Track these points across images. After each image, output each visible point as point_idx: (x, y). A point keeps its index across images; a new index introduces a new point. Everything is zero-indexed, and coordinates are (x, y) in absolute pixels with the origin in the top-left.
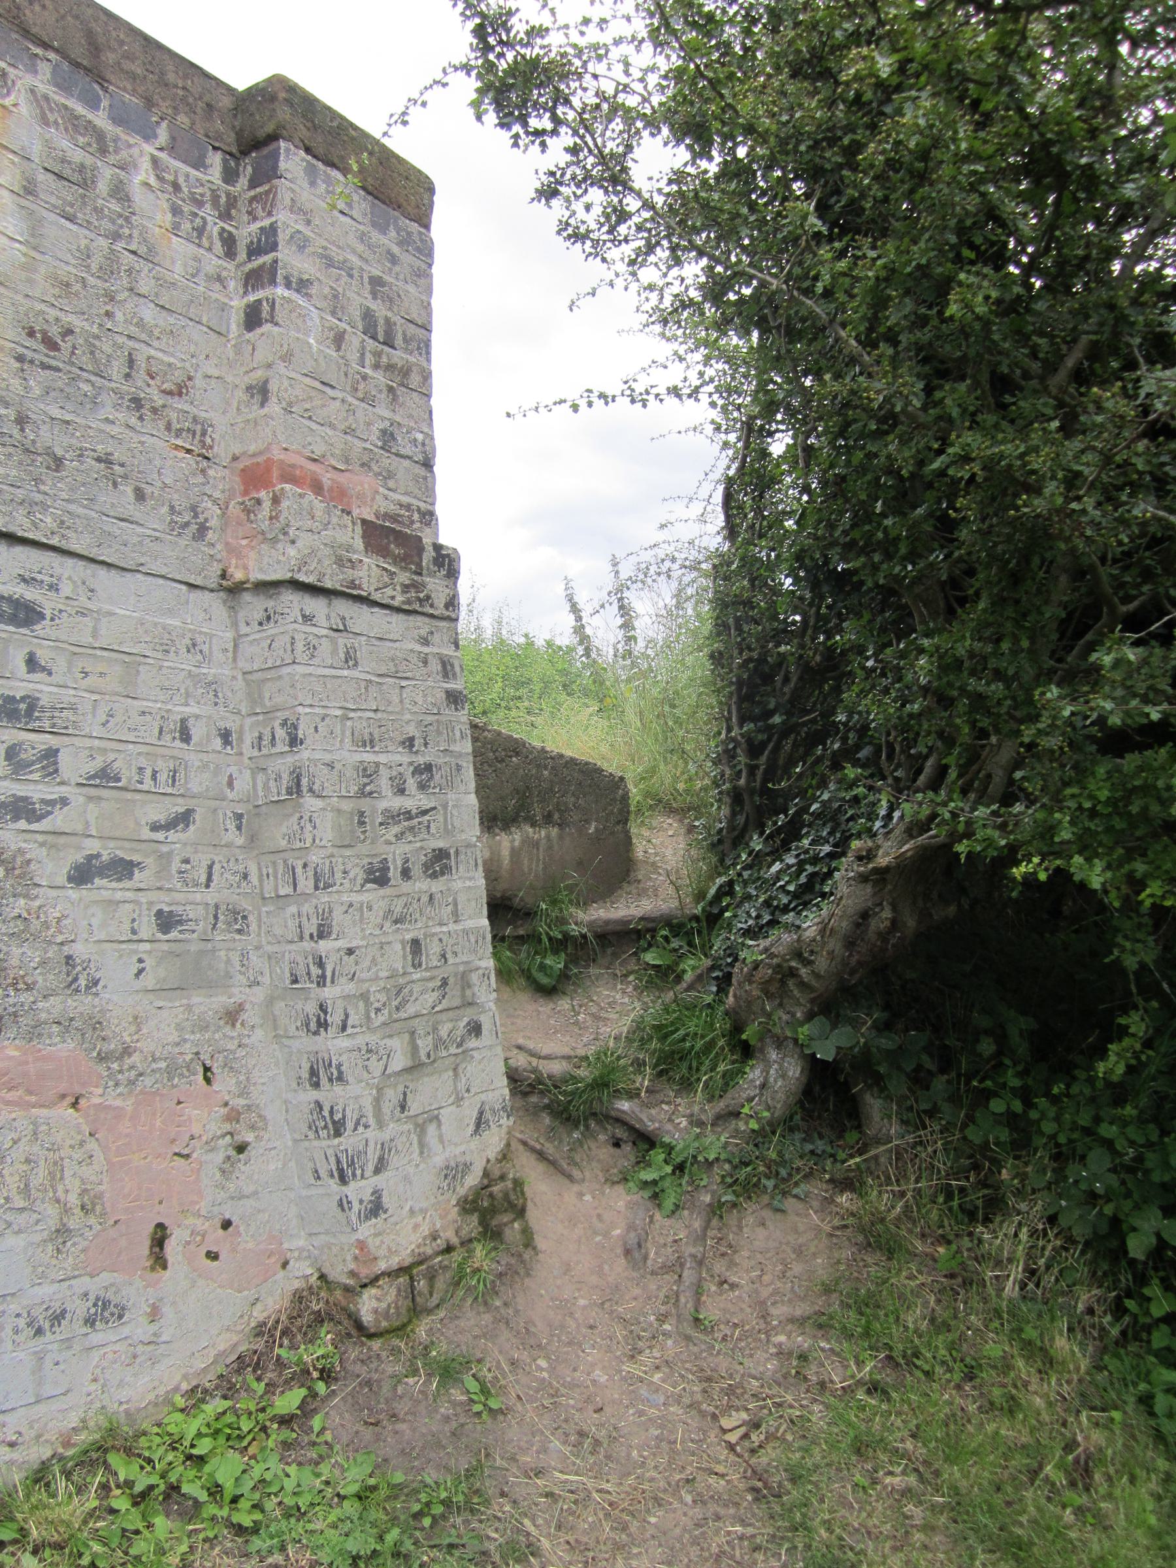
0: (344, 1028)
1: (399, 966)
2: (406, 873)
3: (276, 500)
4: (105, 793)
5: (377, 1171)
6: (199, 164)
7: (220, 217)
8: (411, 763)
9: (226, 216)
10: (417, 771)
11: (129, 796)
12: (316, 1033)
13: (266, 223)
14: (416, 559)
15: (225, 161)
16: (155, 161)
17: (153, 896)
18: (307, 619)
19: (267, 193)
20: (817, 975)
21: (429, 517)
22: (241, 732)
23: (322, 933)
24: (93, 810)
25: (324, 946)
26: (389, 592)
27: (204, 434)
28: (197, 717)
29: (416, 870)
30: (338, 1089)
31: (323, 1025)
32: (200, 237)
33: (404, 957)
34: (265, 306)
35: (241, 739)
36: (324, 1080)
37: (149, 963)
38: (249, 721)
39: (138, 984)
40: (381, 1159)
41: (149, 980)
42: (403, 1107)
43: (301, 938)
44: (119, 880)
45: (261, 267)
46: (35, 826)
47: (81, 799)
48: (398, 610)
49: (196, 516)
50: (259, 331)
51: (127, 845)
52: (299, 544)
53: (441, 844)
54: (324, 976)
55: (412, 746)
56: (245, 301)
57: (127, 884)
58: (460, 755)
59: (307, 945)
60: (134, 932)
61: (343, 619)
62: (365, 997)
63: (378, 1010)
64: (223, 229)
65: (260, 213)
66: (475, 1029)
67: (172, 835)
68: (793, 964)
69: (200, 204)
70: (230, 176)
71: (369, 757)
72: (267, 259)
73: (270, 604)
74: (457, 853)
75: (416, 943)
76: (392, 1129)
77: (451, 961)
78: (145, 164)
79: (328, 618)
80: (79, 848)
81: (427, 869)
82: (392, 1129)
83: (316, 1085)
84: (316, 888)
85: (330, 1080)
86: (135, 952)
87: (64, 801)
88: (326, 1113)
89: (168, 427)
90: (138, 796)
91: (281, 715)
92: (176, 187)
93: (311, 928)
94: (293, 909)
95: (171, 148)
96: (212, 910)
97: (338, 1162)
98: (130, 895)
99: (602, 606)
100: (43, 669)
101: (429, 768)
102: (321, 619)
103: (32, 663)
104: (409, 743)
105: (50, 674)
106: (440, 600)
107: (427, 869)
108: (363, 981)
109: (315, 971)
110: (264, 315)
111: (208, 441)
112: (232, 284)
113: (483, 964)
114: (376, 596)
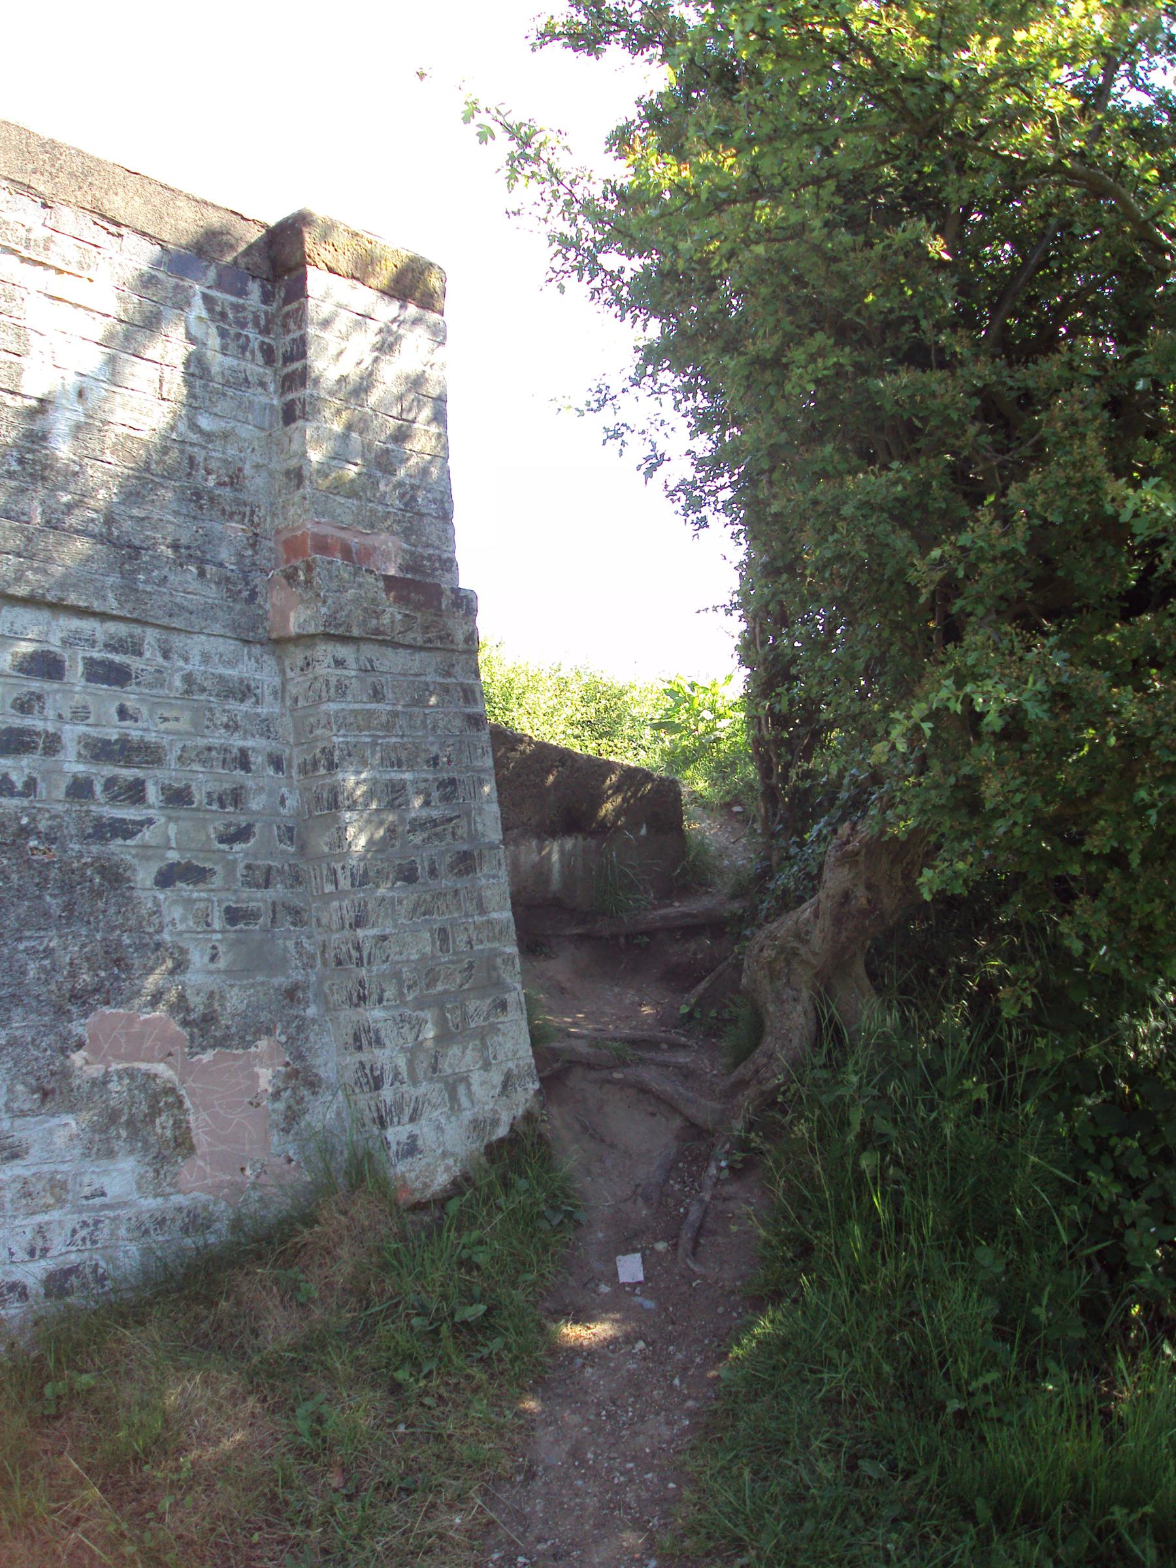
0: (380, 1001)
1: (428, 949)
2: (433, 872)
3: (309, 568)
4: (182, 813)
5: (412, 1120)
6: (242, 292)
7: (260, 333)
8: (435, 780)
9: (266, 331)
10: (442, 785)
11: (201, 815)
12: (357, 1005)
13: (296, 335)
14: (436, 603)
15: (263, 286)
16: (206, 298)
17: (223, 895)
18: (339, 663)
19: (297, 310)
20: (815, 954)
21: (449, 565)
22: (290, 760)
23: (359, 923)
24: (172, 829)
25: (360, 933)
26: (412, 635)
27: (253, 513)
28: (254, 749)
29: (442, 869)
30: (377, 1051)
31: (363, 998)
32: (243, 353)
33: (433, 943)
34: (298, 407)
35: (290, 766)
36: (365, 1042)
37: (221, 949)
38: (296, 751)
39: (212, 967)
40: (415, 1110)
41: (222, 964)
42: (435, 1070)
43: (343, 928)
44: (195, 883)
45: (294, 372)
46: (129, 842)
47: (163, 820)
48: (421, 649)
49: (247, 584)
50: (293, 426)
51: (201, 855)
52: (330, 601)
53: (465, 847)
54: (361, 958)
55: (436, 764)
56: (322, 334)
57: (201, 886)
58: (483, 770)
59: (347, 933)
60: (208, 925)
61: (371, 661)
62: (397, 975)
63: (409, 987)
64: (263, 343)
65: (292, 326)
66: (503, 1006)
67: (237, 847)
68: (795, 945)
69: (243, 325)
70: (267, 298)
71: (396, 776)
72: (297, 365)
73: (309, 653)
74: (481, 854)
75: (443, 931)
76: (424, 1088)
77: (476, 948)
78: (198, 301)
79: (357, 660)
80: (163, 858)
81: (453, 868)
82: (424, 1088)
83: (360, 1048)
84: (353, 885)
85: (370, 1044)
86: (210, 940)
87: (150, 821)
88: (368, 1071)
89: (223, 512)
90: (208, 816)
91: (321, 745)
92: (223, 315)
93: (349, 918)
94: (335, 904)
95: (219, 285)
96: (270, 907)
97: (378, 1110)
98: (204, 895)
99: (715, 609)
100: (132, 717)
101: (452, 781)
102: (351, 661)
103: (123, 713)
104: (435, 761)
105: (136, 720)
106: (460, 637)
107: (453, 868)
108: (397, 962)
109: (355, 954)
110: (298, 413)
111: (256, 519)
112: (272, 388)
113: (508, 950)
114: (399, 639)
